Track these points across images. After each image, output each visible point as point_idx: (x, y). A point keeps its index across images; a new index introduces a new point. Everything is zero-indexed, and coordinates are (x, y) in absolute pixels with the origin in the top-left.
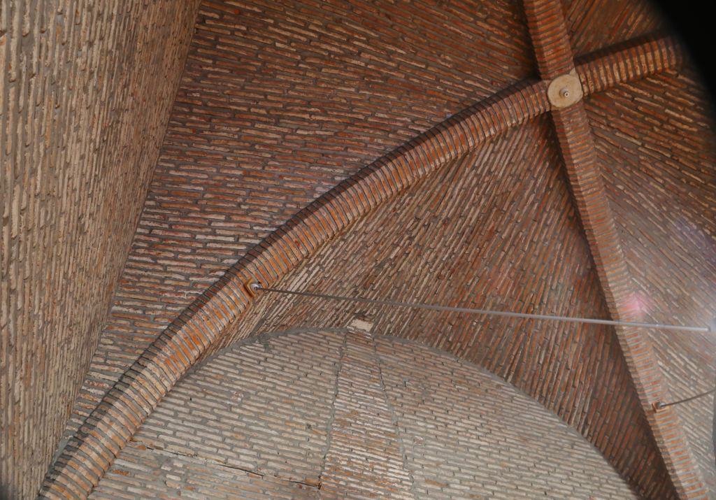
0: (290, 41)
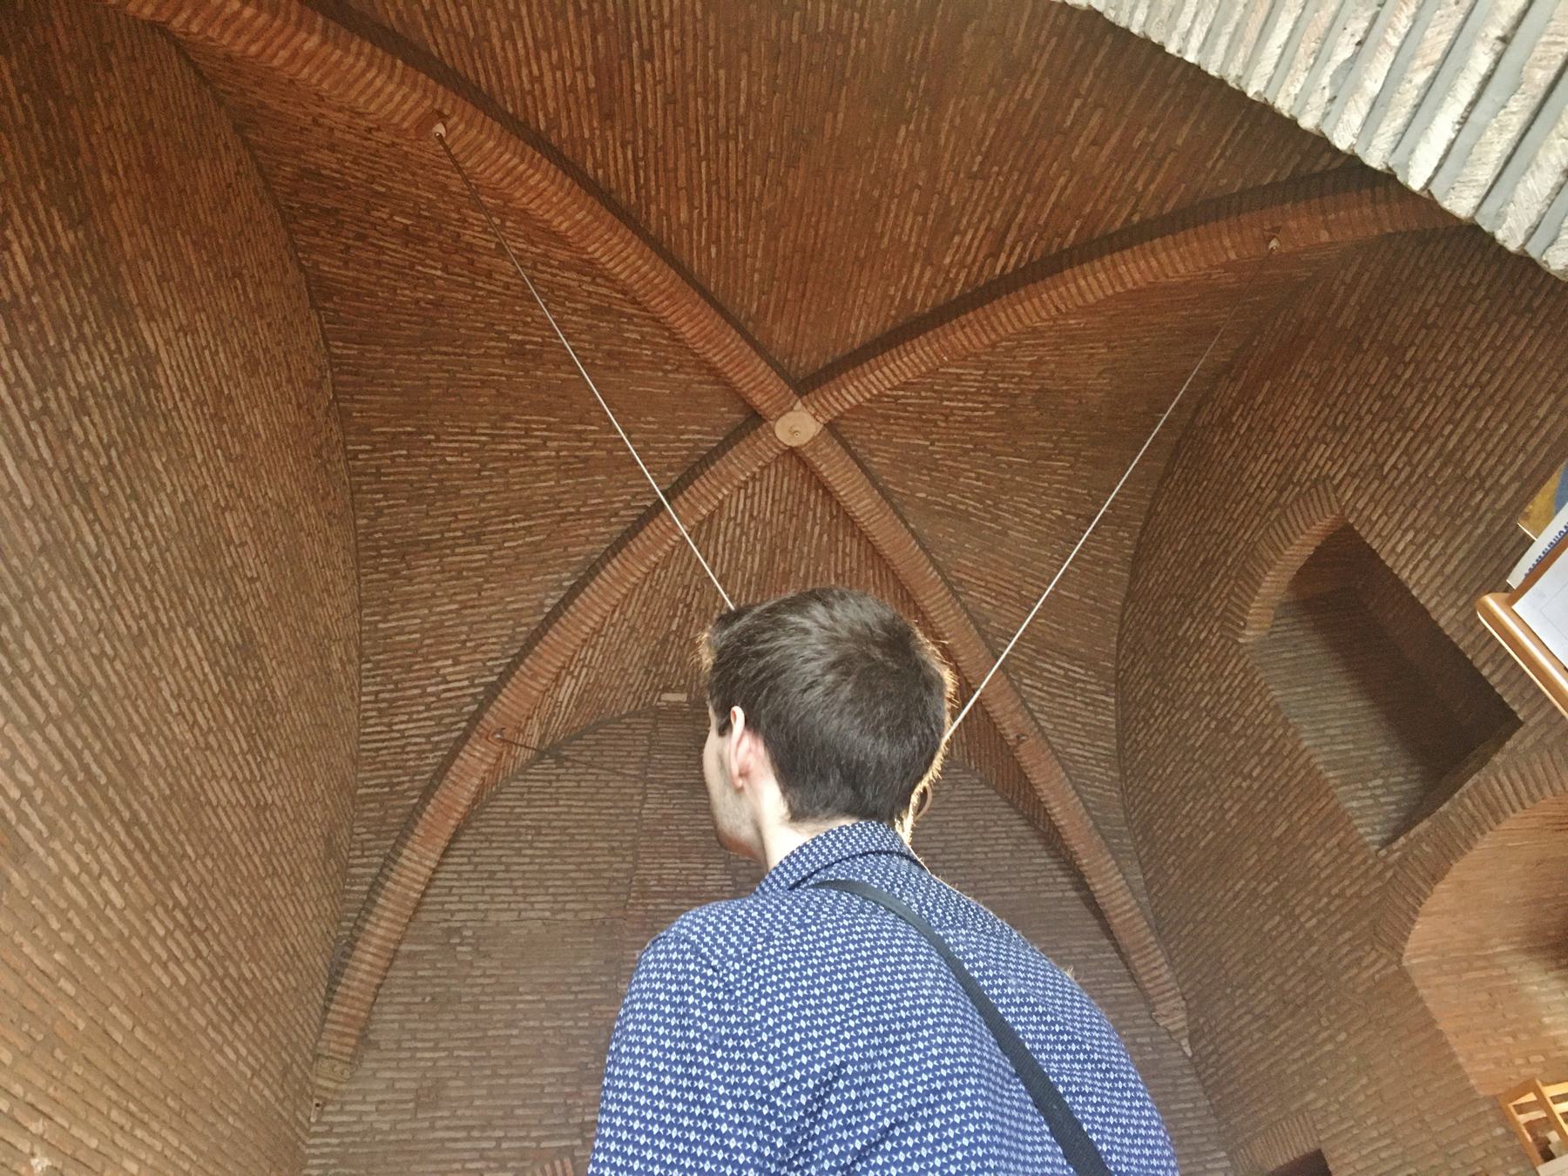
0: (460, 452)
